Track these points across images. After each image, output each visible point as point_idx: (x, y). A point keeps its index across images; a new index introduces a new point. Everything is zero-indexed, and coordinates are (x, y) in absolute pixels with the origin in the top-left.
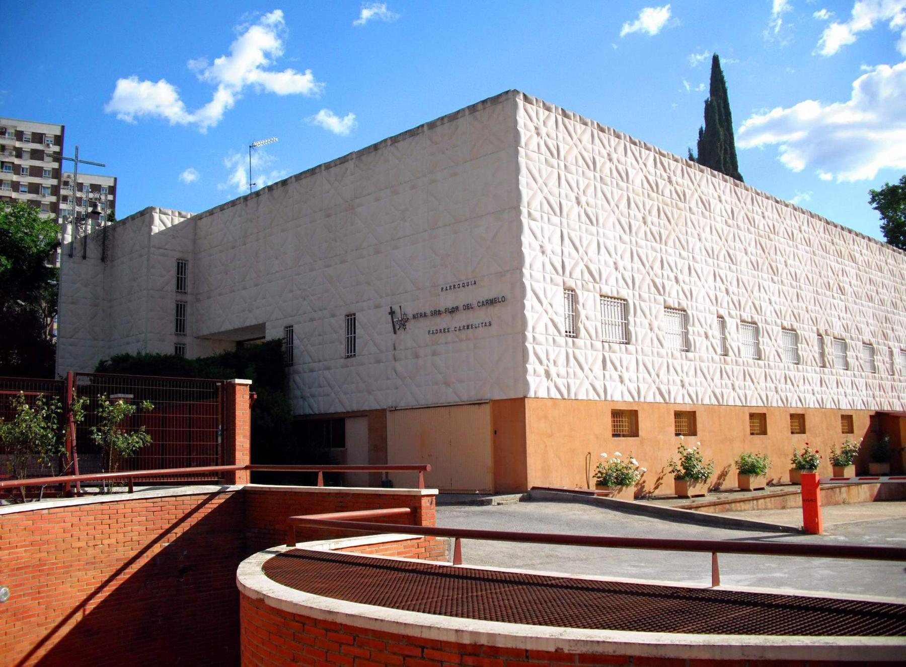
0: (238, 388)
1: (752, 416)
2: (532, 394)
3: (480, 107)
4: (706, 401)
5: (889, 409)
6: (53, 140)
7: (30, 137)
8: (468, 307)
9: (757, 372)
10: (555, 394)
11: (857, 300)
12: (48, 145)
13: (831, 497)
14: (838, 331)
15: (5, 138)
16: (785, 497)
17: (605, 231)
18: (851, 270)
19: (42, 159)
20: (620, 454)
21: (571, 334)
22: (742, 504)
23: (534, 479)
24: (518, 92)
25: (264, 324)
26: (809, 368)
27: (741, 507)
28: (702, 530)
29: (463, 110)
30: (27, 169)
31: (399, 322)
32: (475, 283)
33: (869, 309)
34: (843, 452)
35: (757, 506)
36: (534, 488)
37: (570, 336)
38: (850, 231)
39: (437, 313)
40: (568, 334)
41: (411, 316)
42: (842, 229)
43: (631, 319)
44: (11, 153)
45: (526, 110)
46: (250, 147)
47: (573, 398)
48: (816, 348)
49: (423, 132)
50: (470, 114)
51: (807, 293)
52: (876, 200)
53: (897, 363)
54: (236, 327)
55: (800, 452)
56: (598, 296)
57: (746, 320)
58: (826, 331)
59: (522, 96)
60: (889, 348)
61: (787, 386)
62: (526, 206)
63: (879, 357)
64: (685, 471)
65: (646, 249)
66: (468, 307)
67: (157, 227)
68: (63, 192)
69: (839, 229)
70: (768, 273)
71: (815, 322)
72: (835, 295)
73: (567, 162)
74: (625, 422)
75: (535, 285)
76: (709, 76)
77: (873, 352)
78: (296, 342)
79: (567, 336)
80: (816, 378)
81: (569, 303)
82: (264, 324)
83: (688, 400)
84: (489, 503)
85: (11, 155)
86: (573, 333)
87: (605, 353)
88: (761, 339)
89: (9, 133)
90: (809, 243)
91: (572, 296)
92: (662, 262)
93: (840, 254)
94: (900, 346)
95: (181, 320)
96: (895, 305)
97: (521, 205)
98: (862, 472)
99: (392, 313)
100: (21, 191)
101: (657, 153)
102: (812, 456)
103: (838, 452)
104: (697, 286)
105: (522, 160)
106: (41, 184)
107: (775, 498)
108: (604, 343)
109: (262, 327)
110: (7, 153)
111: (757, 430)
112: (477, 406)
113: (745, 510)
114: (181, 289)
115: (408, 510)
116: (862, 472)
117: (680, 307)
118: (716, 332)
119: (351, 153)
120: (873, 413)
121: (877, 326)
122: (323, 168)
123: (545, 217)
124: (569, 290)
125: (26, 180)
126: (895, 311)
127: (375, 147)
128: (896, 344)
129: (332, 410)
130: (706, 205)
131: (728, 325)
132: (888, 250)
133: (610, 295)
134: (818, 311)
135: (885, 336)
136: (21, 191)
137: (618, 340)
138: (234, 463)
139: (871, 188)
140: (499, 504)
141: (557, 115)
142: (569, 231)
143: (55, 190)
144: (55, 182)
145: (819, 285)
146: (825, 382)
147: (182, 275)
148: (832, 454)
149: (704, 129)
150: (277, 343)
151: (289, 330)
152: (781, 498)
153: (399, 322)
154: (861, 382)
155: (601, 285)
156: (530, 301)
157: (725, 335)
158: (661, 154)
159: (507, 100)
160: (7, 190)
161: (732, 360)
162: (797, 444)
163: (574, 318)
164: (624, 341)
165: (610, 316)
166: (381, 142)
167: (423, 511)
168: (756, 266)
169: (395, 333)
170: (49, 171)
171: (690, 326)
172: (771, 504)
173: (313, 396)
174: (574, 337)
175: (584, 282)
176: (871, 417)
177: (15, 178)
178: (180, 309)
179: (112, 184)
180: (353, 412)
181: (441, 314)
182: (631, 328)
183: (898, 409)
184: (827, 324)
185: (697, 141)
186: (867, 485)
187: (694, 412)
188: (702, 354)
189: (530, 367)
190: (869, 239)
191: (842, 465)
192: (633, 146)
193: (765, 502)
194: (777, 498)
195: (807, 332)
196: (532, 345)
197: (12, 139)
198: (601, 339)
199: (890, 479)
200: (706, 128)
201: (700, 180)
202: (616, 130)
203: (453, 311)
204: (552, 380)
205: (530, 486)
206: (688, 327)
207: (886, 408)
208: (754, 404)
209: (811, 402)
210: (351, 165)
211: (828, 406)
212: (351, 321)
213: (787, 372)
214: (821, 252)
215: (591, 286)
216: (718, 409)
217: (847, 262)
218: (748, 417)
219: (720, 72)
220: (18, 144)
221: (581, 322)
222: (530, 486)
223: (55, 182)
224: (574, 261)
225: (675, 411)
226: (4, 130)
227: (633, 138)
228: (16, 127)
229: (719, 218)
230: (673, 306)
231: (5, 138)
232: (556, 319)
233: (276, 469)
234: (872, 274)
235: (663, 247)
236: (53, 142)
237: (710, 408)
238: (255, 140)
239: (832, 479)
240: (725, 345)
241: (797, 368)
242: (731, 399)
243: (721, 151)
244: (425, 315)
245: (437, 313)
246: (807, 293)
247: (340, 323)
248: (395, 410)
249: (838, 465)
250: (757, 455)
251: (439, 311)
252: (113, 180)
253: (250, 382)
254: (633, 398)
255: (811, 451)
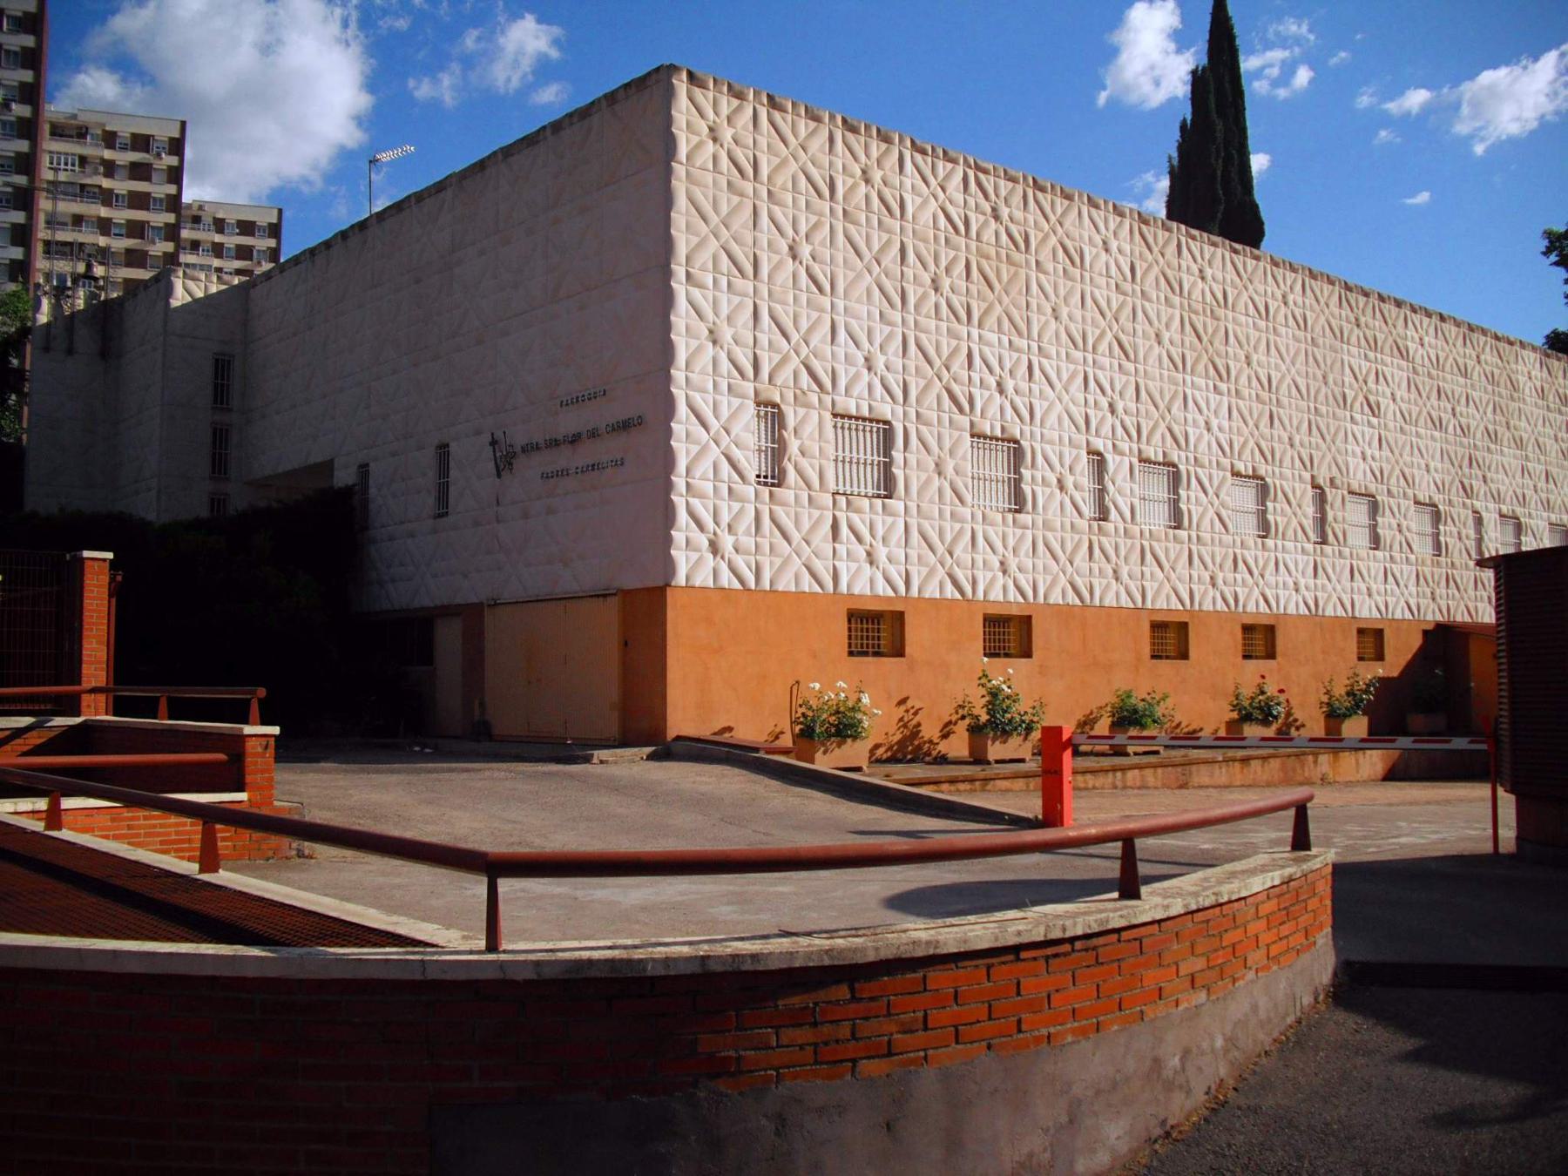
0: (87, 563)
1: (1361, 631)
2: (680, 579)
3: (621, 94)
4: (1056, 598)
5: (1467, 619)
6: (167, 146)
7: (129, 142)
8: (594, 434)
9: (1171, 548)
10: (727, 580)
11: (1407, 427)
12: (159, 155)
13: (1294, 770)
14: (1360, 476)
15: (85, 143)
16: (1188, 767)
17: (848, 303)
18: (1396, 370)
19: (148, 179)
20: (845, 686)
21: (769, 480)
22: (1088, 776)
23: (681, 721)
24: (673, 69)
25: (331, 461)
26: (1290, 545)
27: (1085, 782)
28: (872, 816)
29: (599, 100)
30: (123, 196)
31: (505, 461)
32: (604, 394)
33: (1431, 441)
34: (1348, 694)
35: (1124, 780)
36: (678, 738)
37: (766, 484)
38: (1399, 304)
39: (554, 443)
40: (762, 479)
41: (518, 449)
42: (1382, 298)
43: (898, 455)
44: (96, 169)
45: (691, 99)
46: (371, 162)
47: (683, 584)
48: (1310, 510)
49: (545, 138)
50: (609, 106)
51: (1293, 412)
52: (1555, 249)
53: (1490, 540)
54: (297, 467)
55: (1247, 691)
56: (828, 416)
57: (1153, 458)
58: (1332, 480)
59: (684, 76)
60: (1475, 512)
61: (1238, 576)
62: (684, 261)
63: (1450, 528)
64: (988, 717)
65: (936, 333)
66: (594, 434)
67: (179, 298)
68: (185, 234)
69: (1374, 300)
70: (1207, 376)
71: (1308, 463)
72: (1358, 417)
73: (774, 186)
74: (1259, 640)
75: (697, 398)
76: (1208, 27)
77: (1437, 517)
78: (373, 491)
79: (759, 483)
80: (1306, 562)
81: (766, 427)
82: (331, 461)
83: (1013, 595)
84: (587, 760)
85: (96, 173)
86: (774, 477)
87: (837, 513)
88: (1182, 492)
89: (92, 135)
90: (1303, 324)
91: (773, 416)
92: (970, 356)
93: (1374, 345)
94: (1500, 510)
95: (220, 454)
96: (1493, 437)
97: (672, 261)
98: (1380, 731)
99: (494, 443)
100: (115, 235)
101: (970, 167)
102: (1271, 699)
103: (1339, 690)
104: (1046, 399)
105: (680, 187)
106: (148, 222)
107: (1165, 769)
108: (838, 497)
109: (327, 467)
110: (88, 169)
111: (1370, 651)
112: (601, 599)
113: (1094, 788)
114: (222, 403)
115: (222, 756)
116: (1380, 731)
117: (1005, 436)
118: (1083, 476)
119: (450, 176)
120: (1430, 627)
121: (1449, 473)
122: (413, 200)
123: (724, 282)
124: (766, 406)
125: (122, 215)
126: (1493, 446)
127: (481, 165)
128: (1491, 506)
129: (416, 604)
130: (1075, 258)
131: (1111, 466)
132: (1484, 338)
133: (854, 412)
134: (1317, 444)
135: (1467, 491)
136: (115, 235)
137: (870, 492)
138: (80, 684)
139: (1547, 227)
140: (602, 762)
141: (758, 106)
142: (772, 304)
143: (172, 233)
144: (171, 218)
145: (1321, 398)
146: (1324, 569)
147: (223, 379)
148: (1327, 696)
149: (1189, 122)
150: (347, 492)
151: (364, 469)
152: (1179, 769)
153: (505, 461)
154: (1406, 572)
155: (835, 397)
156: (682, 424)
157: (1103, 485)
158: (978, 168)
159: (657, 82)
160: (93, 233)
161: (1116, 528)
162: (1249, 676)
163: (777, 452)
164: (882, 492)
165: (862, 451)
166: (489, 157)
167: (249, 760)
168: (1179, 365)
169: (499, 476)
170: (161, 200)
171: (1026, 468)
172: (1156, 778)
173: (393, 581)
174: (773, 485)
175: (798, 391)
176: (1425, 633)
177: (104, 212)
178: (220, 436)
179: (275, 221)
180: (443, 607)
181: (558, 445)
182: (898, 472)
183: (1459, 619)
184: (1334, 468)
185: (1176, 144)
186: (1379, 751)
187: (1030, 617)
188: (1050, 516)
189: (678, 536)
190: (1442, 318)
191: (1339, 716)
192: (918, 157)
193: (1142, 776)
194: (1170, 768)
195: (1291, 482)
196: (684, 500)
197: (97, 145)
198: (832, 486)
199: (1415, 742)
200: (1192, 120)
201: (1064, 214)
202: (882, 129)
203: (575, 439)
204: (723, 558)
205: (671, 733)
206: (1022, 470)
207: (1461, 617)
208: (1161, 604)
209: (1291, 604)
210: (448, 194)
211: (1329, 612)
212: (443, 451)
213: (1238, 551)
214: (1329, 339)
215: (814, 398)
216: (1315, 620)
217: (1388, 360)
218: (1146, 627)
219: (1227, 19)
220: (108, 154)
221: (789, 460)
222: (671, 733)
223: (171, 218)
224: (780, 356)
225: (984, 614)
226: (84, 131)
227: (918, 142)
228: (104, 125)
229: (1102, 281)
230: (989, 434)
231: (85, 143)
232: (737, 454)
233: (199, 693)
234: (1444, 380)
235: (975, 332)
236: (167, 150)
237: (1064, 611)
238: (379, 152)
239: (1363, 740)
240: (1104, 501)
241: (1263, 544)
242: (1111, 595)
243: (1217, 160)
244: (538, 448)
245: (554, 443)
246: (1293, 412)
247: (428, 457)
248: (495, 604)
249: (1334, 716)
250: (1149, 694)
251: (556, 440)
252: (275, 212)
253: (110, 555)
254: (894, 590)
255: (1271, 690)
